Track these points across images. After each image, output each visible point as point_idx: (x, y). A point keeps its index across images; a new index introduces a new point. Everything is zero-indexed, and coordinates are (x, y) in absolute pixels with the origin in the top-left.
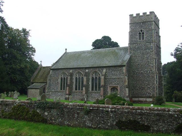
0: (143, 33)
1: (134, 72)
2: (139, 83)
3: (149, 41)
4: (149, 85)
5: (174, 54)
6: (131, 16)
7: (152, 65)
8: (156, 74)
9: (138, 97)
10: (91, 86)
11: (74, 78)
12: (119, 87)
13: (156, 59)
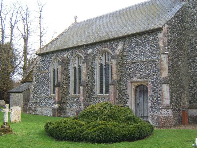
11: (71, 68)
12: (149, 83)
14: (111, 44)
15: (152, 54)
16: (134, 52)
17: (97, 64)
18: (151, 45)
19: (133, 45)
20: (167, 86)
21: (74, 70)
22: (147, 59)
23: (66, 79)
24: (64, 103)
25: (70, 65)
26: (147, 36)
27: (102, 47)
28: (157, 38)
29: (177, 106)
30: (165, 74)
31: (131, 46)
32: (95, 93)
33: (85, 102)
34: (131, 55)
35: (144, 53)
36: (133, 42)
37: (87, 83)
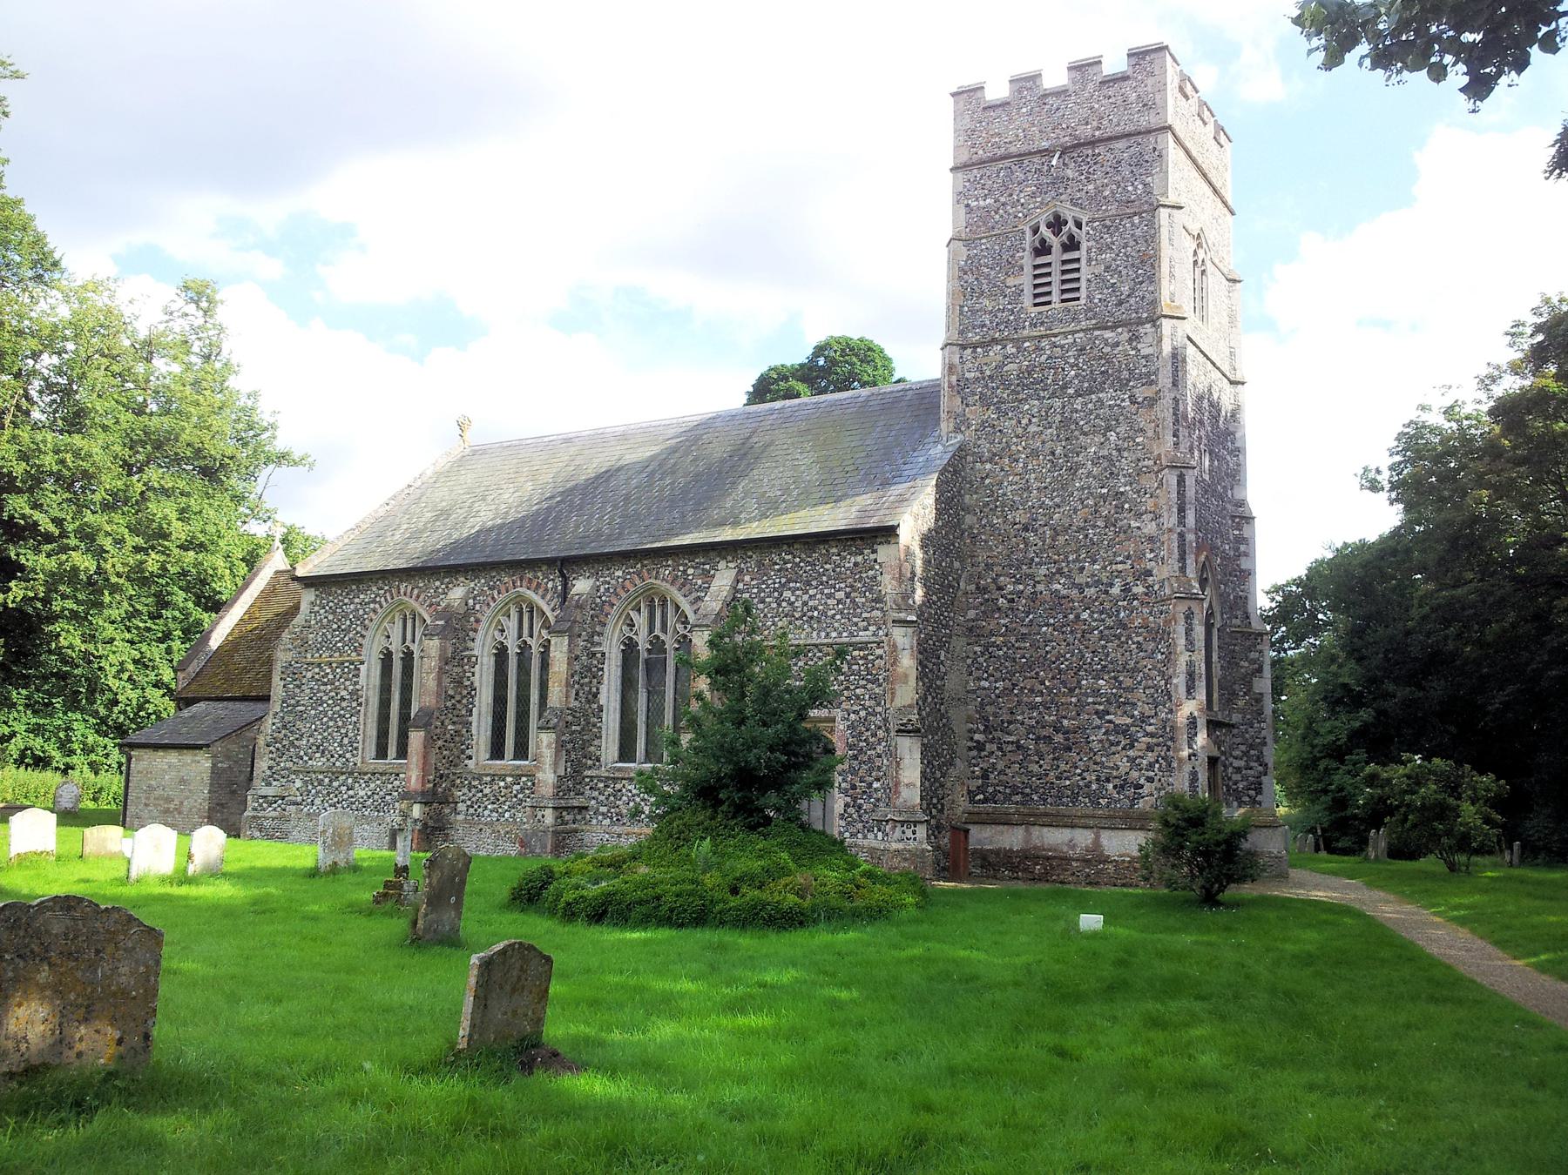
0: (1072, 245)
1: (985, 590)
2: (1032, 690)
3: (1121, 314)
4: (1126, 706)
5: (1384, 478)
6: (967, 96)
7: (1150, 528)
8: (1182, 607)
9: (1029, 820)
10: (611, 722)
11: (482, 649)
12: (841, 726)
13: (1181, 469)
14: (681, 568)
15: (855, 620)
16: (779, 605)
17: (615, 641)
18: (852, 586)
19: (775, 580)
20: (914, 740)
21: (493, 659)
22: (834, 634)
23: (458, 697)
24: (445, 801)
25: (479, 636)
26: (834, 550)
27: (639, 574)
28: (875, 561)
29: (934, 812)
30: (907, 694)
31: (770, 582)
32: (598, 760)
33: (561, 794)
34: (765, 616)
35: (824, 613)
36: (777, 567)
37: (570, 718)
